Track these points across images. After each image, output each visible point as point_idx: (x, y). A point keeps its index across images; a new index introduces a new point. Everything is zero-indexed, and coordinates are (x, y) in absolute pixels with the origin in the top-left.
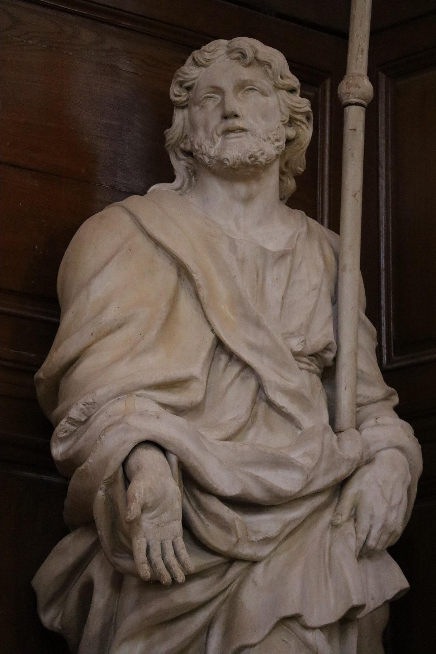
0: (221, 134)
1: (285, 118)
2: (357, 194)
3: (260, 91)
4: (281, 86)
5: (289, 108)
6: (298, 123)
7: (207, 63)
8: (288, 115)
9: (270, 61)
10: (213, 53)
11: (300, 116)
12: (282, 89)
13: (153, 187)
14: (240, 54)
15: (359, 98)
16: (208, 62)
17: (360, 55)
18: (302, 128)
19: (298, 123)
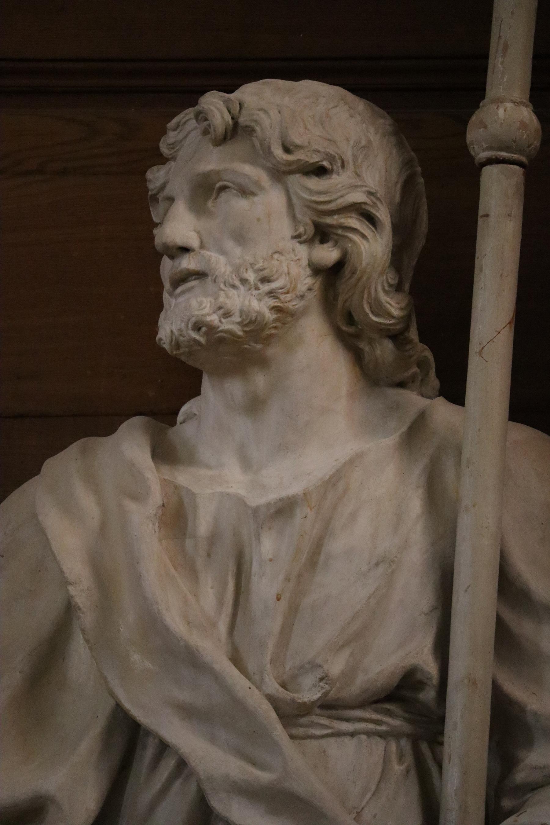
0: (171, 289)
1: (301, 229)
2: (485, 349)
3: (236, 188)
4: (284, 168)
5: (308, 207)
6: (340, 232)
7: (173, 151)
8: (309, 221)
9: (253, 124)
10: (179, 129)
11: (336, 217)
12: (291, 172)
13: (185, 408)
14: (230, 122)
15: (491, 148)
16: (173, 148)
17: (500, 58)
18: (351, 240)
19: (340, 232)
